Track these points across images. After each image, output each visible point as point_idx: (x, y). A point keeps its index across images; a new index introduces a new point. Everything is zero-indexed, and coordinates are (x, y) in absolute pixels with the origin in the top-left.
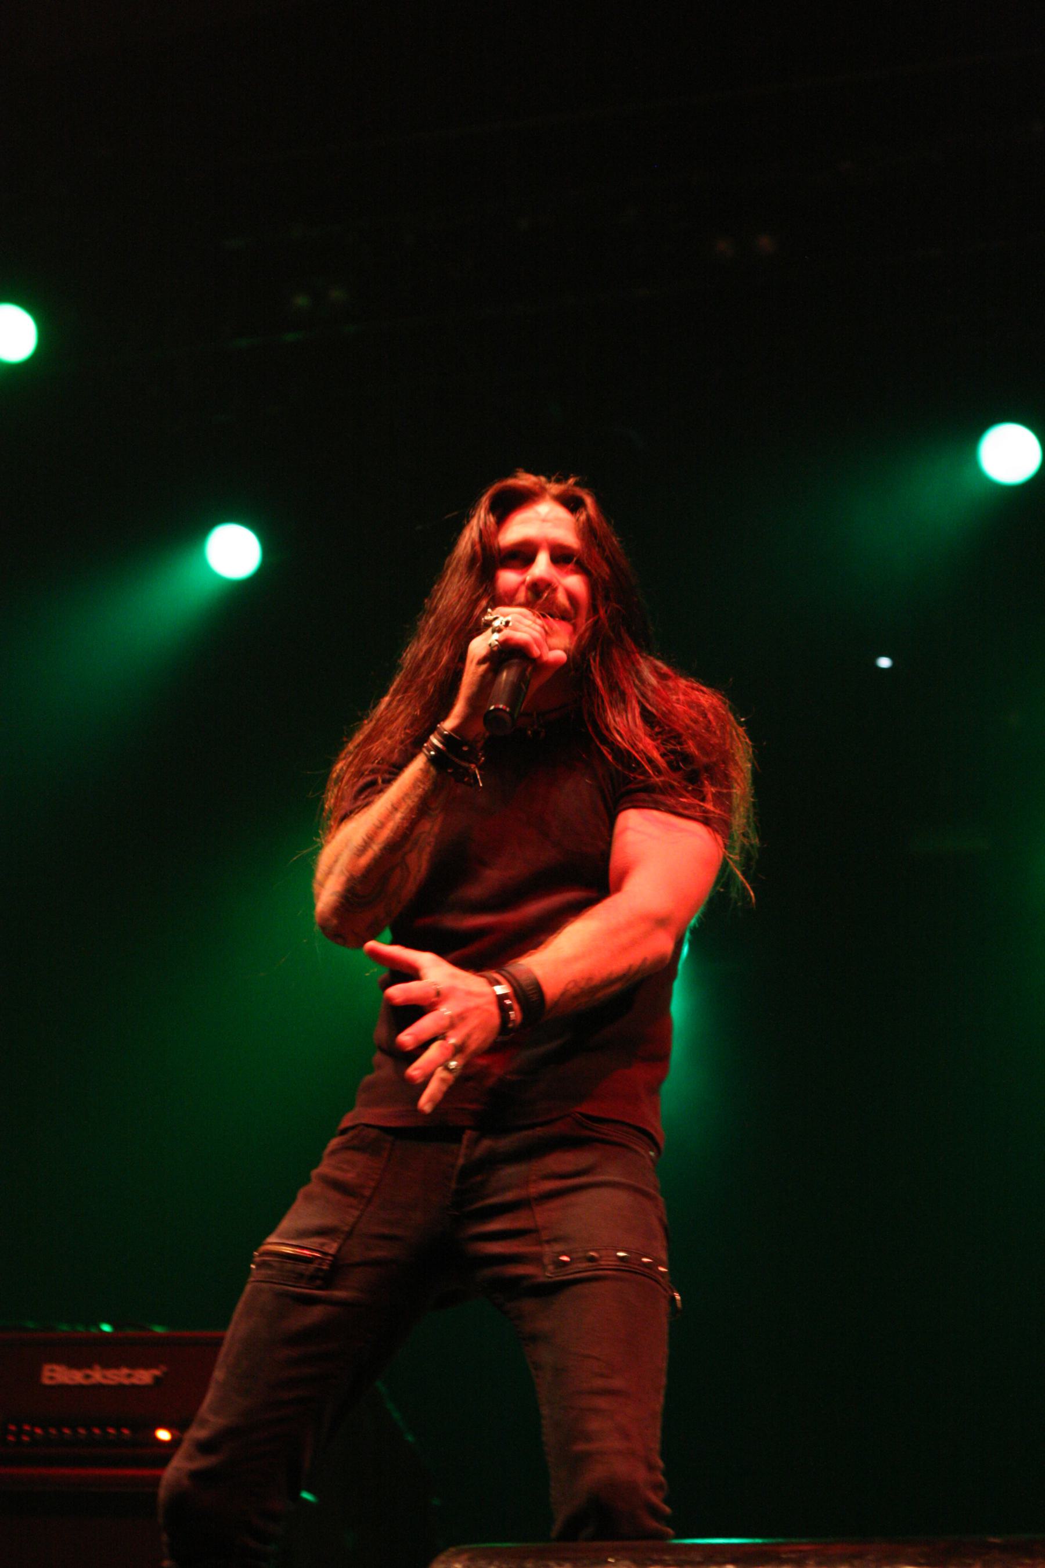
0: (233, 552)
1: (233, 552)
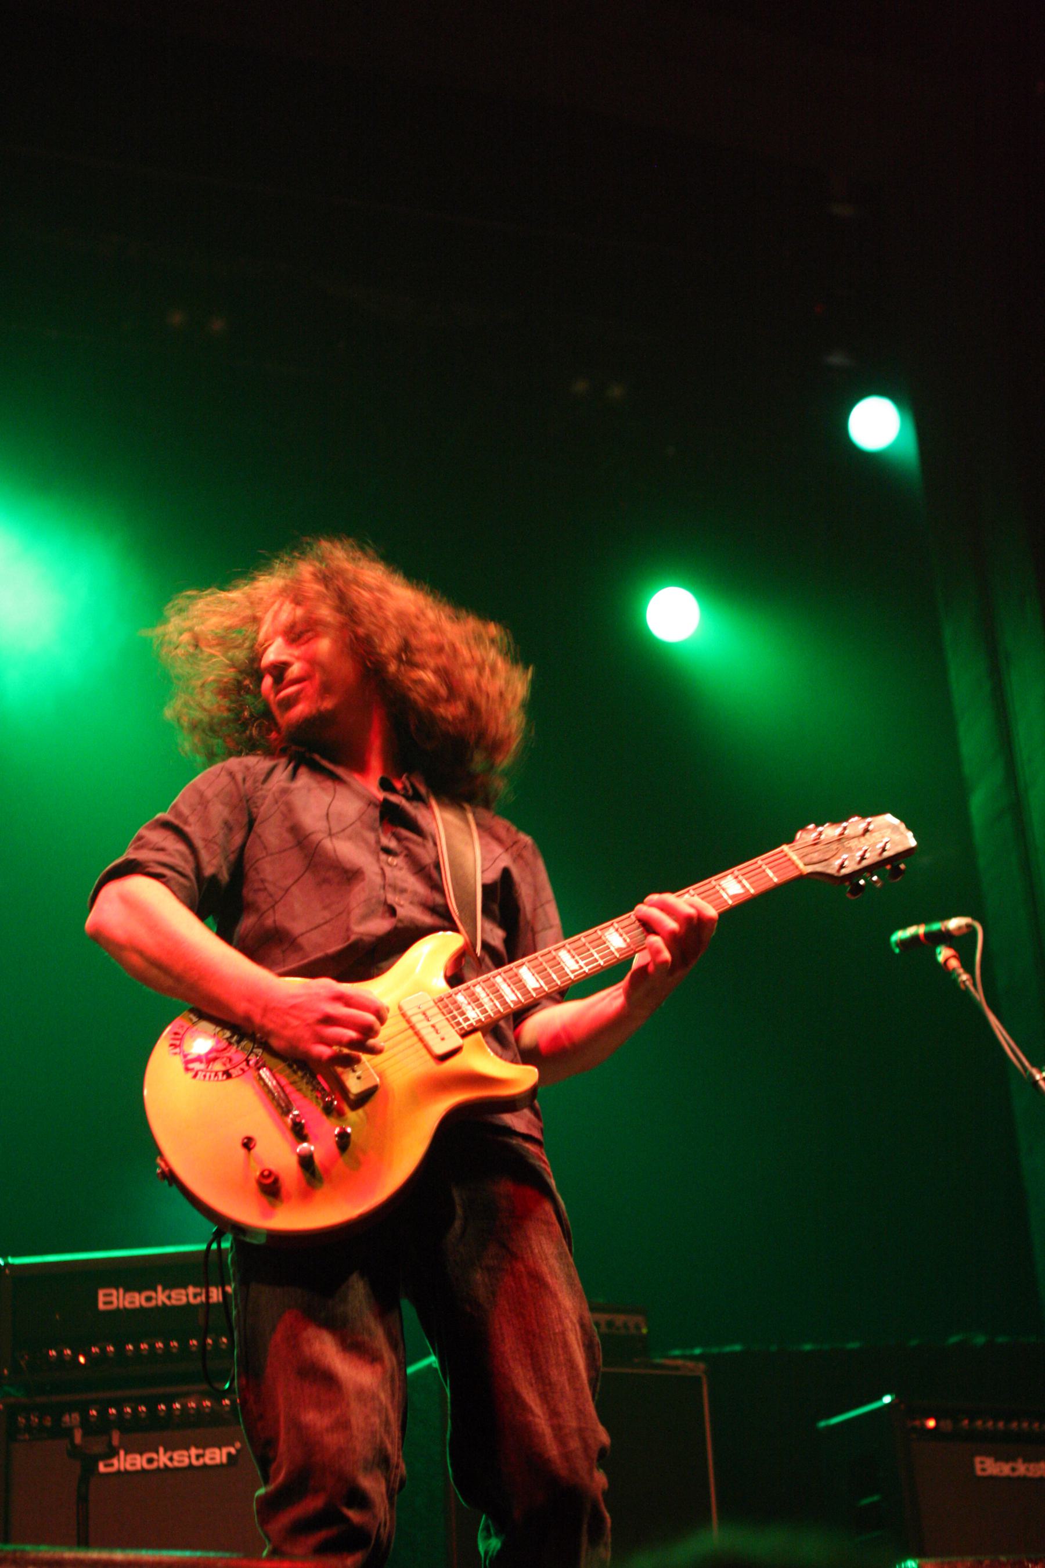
0: (674, 615)
1: (674, 615)
